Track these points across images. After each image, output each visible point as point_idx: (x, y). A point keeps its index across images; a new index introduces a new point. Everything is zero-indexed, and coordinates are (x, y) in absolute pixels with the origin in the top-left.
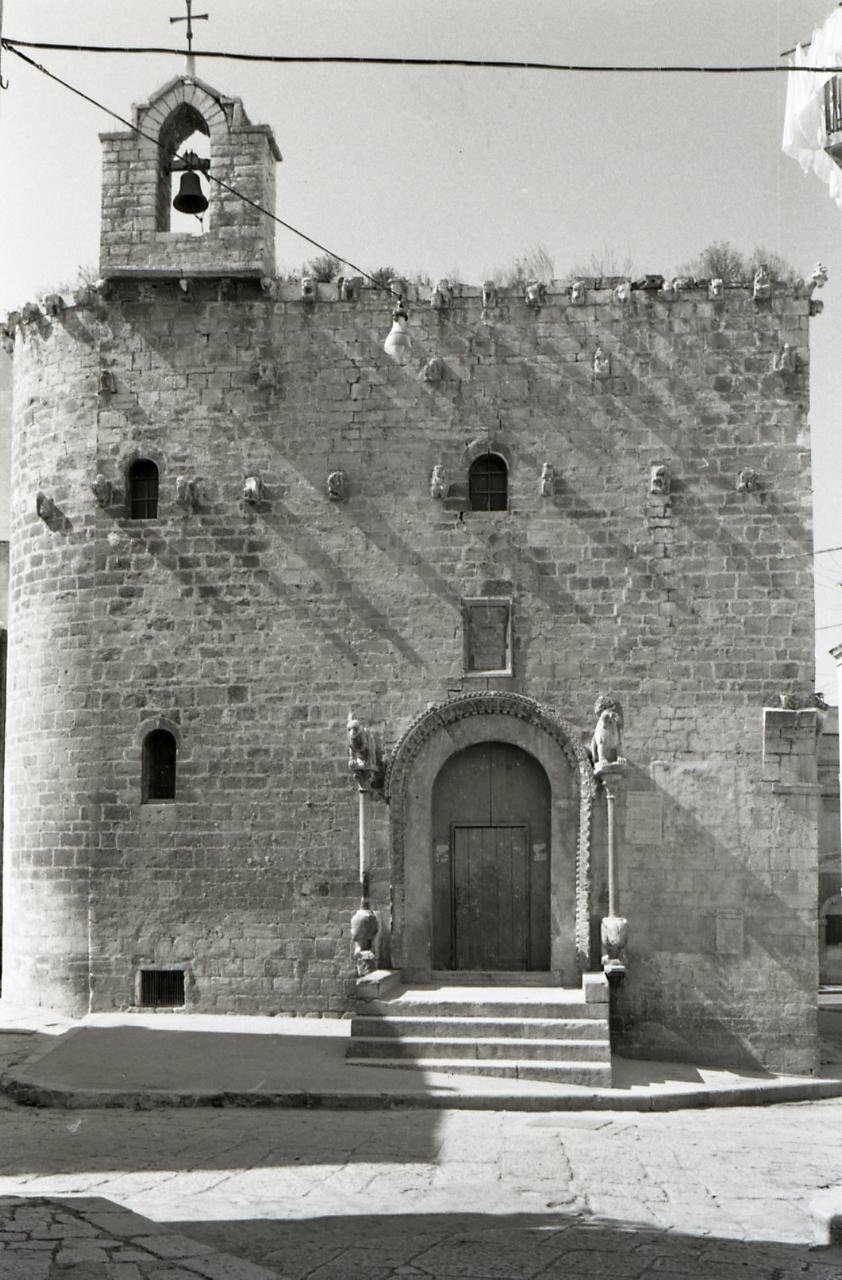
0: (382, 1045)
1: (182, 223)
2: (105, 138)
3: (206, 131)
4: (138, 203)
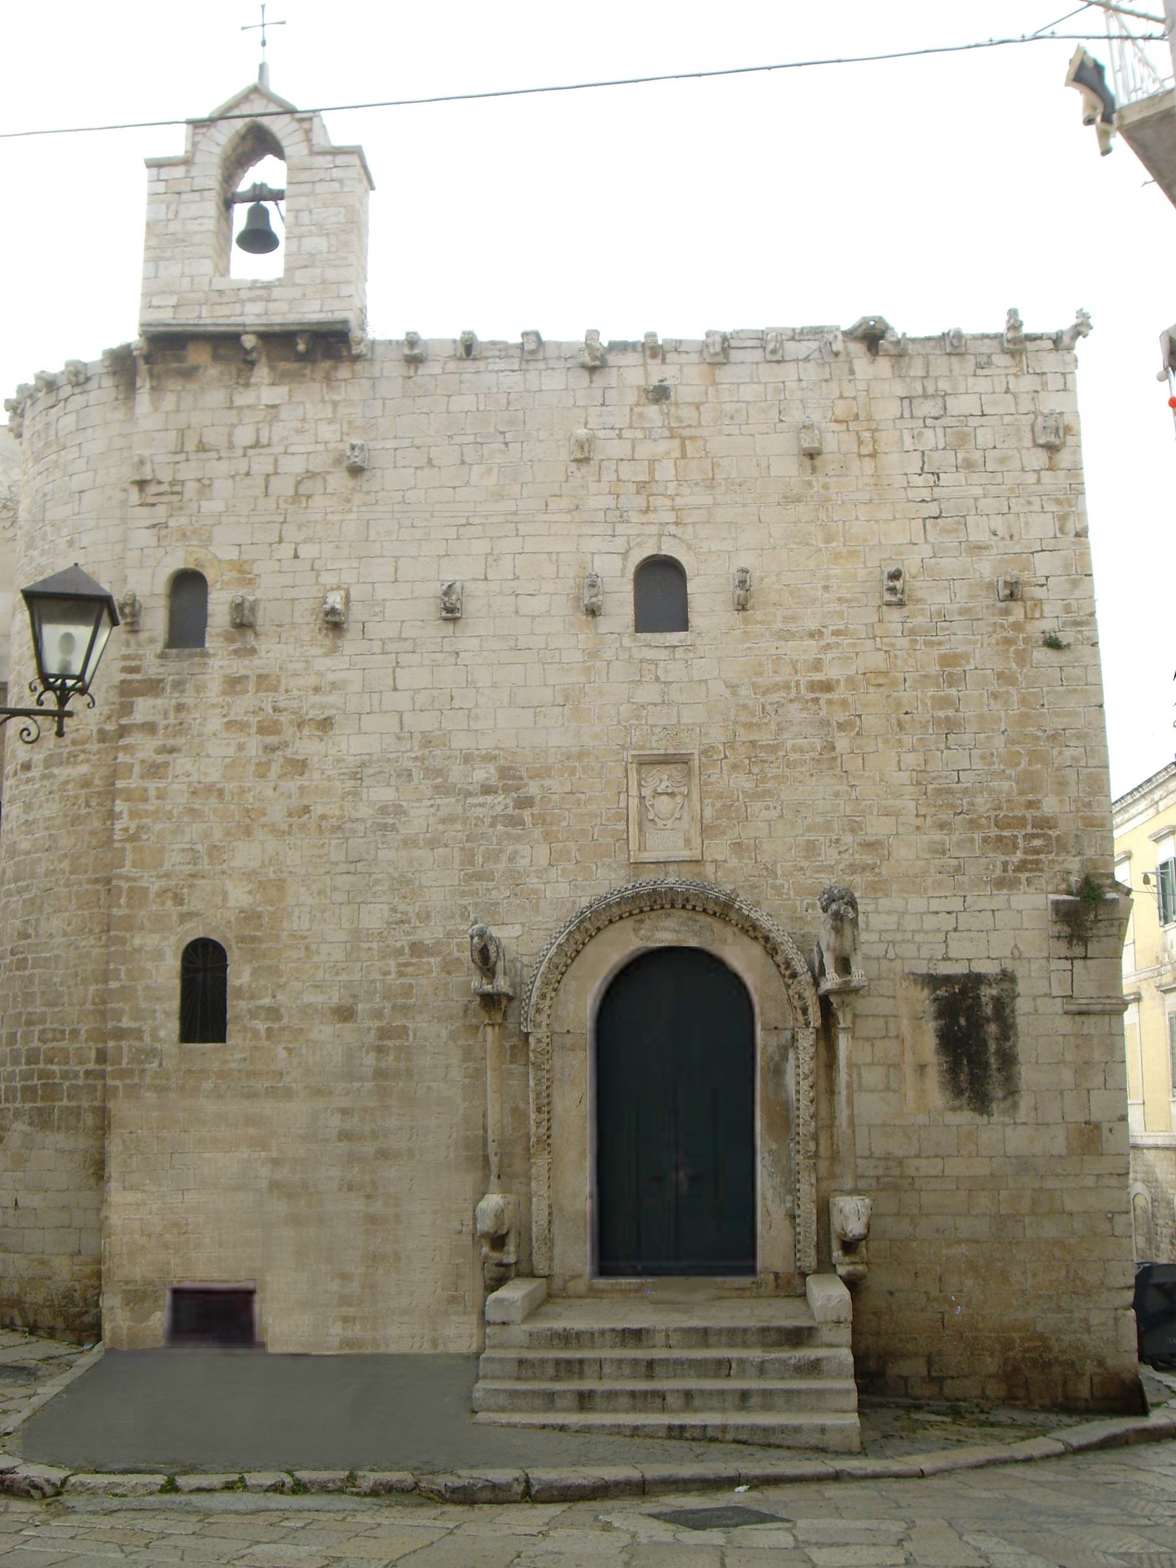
2: (155, 165)
3: (279, 153)
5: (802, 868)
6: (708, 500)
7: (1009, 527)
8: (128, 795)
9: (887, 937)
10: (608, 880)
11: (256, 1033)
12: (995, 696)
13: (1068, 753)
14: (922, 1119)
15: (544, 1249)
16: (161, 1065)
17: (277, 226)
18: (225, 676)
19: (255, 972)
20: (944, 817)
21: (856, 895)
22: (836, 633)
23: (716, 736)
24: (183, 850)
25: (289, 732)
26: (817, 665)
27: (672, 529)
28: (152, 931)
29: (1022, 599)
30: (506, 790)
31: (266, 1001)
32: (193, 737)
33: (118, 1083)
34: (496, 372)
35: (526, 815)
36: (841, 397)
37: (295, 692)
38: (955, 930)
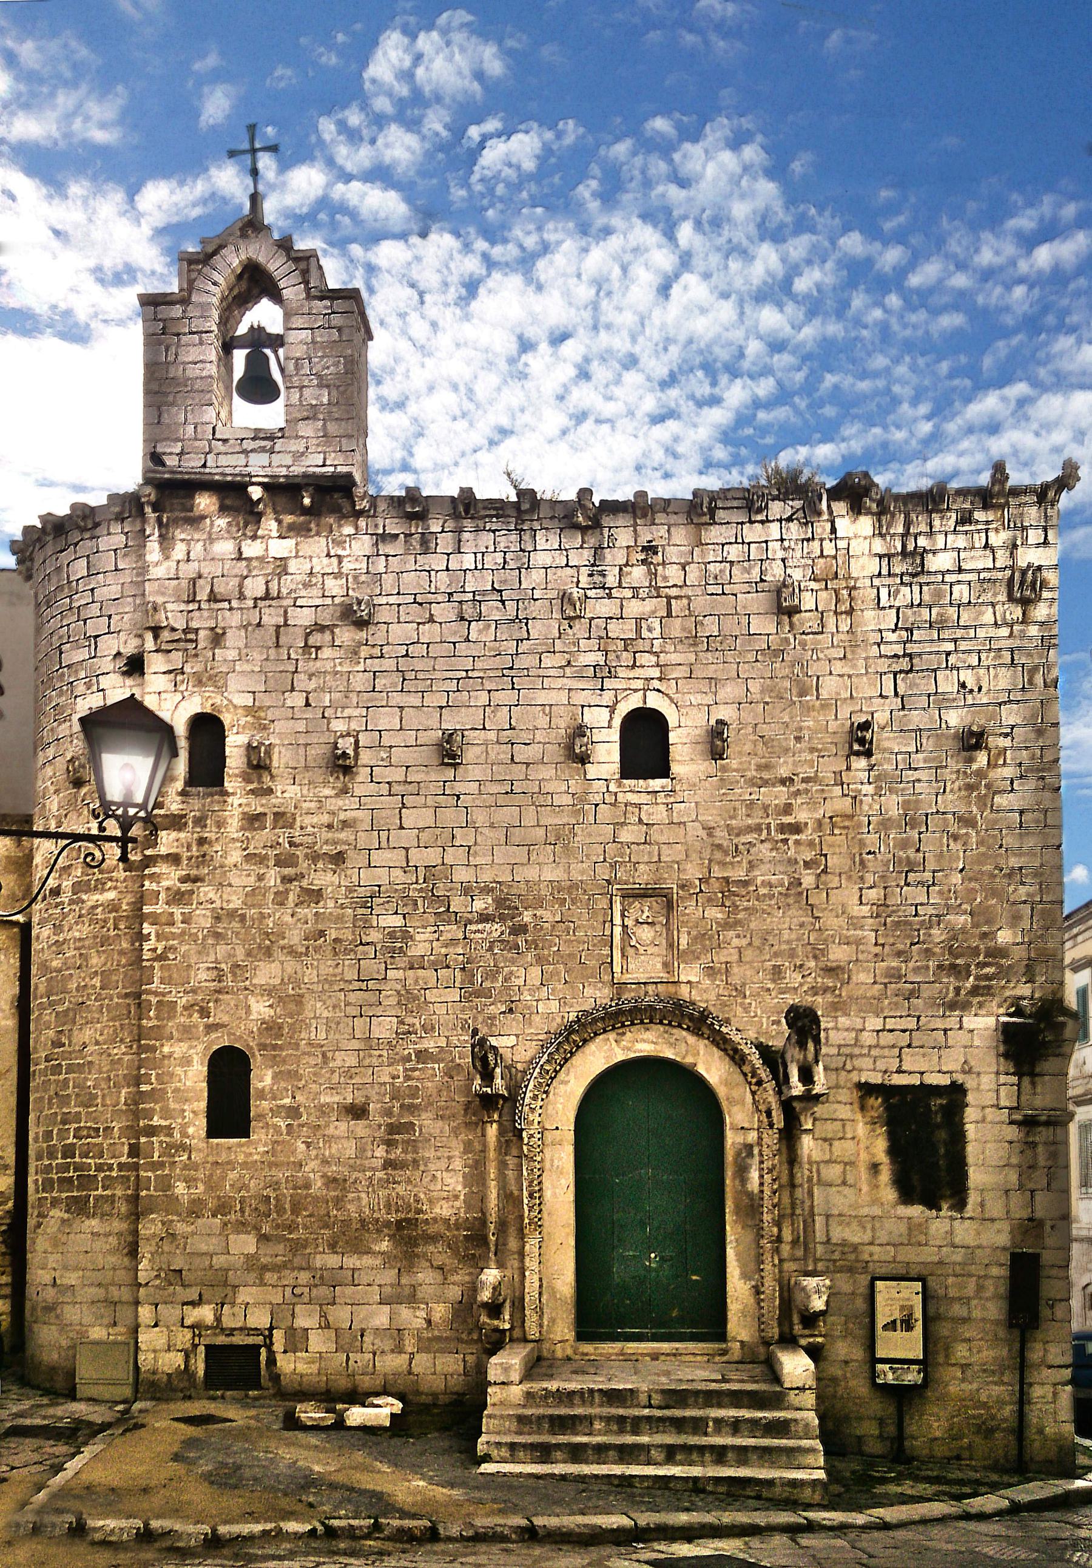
3: (276, 296)
5: (768, 990)
6: (692, 658)
7: (978, 680)
8: (155, 919)
12: (955, 837)
13: (1023, 890)
14: (876, 1211)
15: (535, 1318)
16: (189, 1158)
18: (244, 813)
19: (275, 1077)
20: (901, 947)
21: (819, 1013)
22: (804, 780)
23: (693, 872)
24: (208, 969)
25: (303, 865)
26: (787, 809)
27: (656, 684)
28: (180, 1040)
29: (986, 748)
30: (503, 918)
31: (287, 1101)
32: (215, 869)
33: (150, 1174)
34: (494, 531)
35: (520, 941)
36: (822, 556)
37: (310, 829)
38: (909, 1046)
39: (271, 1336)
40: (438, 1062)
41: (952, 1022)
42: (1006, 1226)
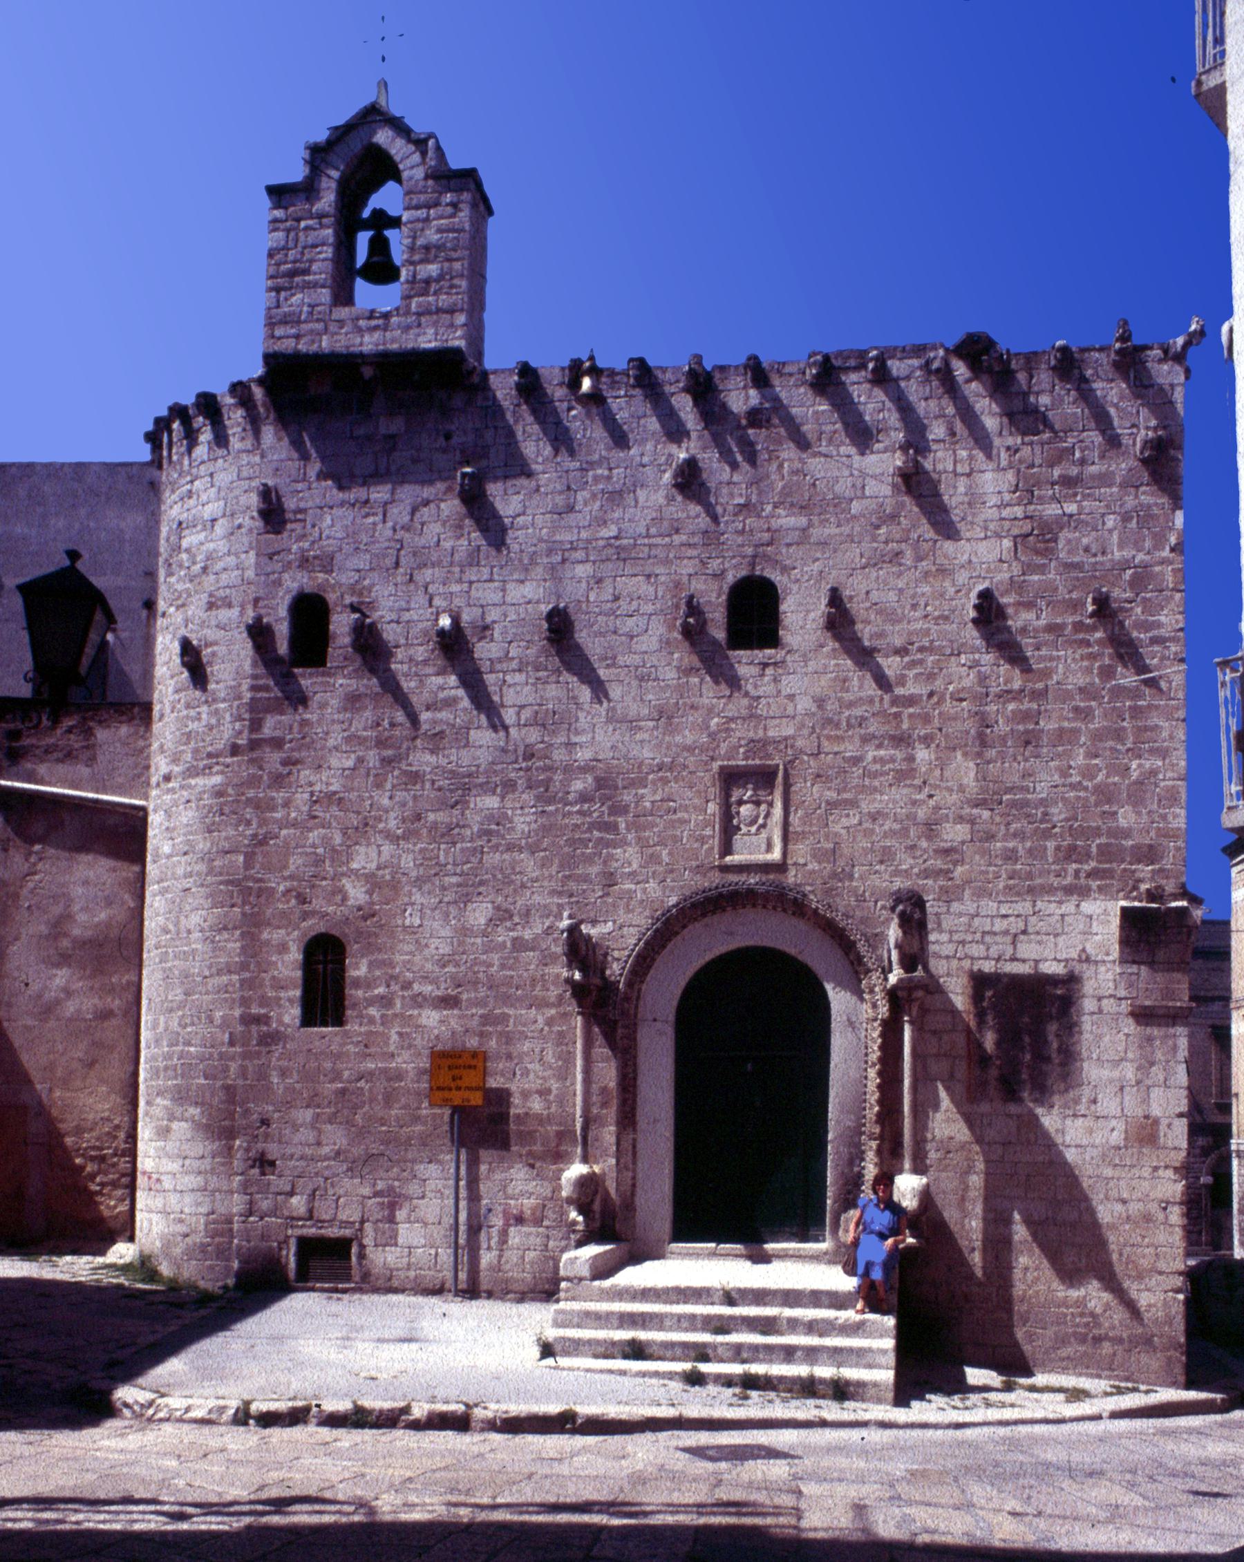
0: (680, 1317)
1: (366, 294)
4: (306, 272)
6: (803, 521)
9: (955, 937)
10: (693, 882)
11: (372, 1021)
17: (398, 254)
19: (371, 965)
22: (921, 649)
39: (361, 1230)
40: (533, 949)
41: (1069, 907)
42: (1120, 1126)
